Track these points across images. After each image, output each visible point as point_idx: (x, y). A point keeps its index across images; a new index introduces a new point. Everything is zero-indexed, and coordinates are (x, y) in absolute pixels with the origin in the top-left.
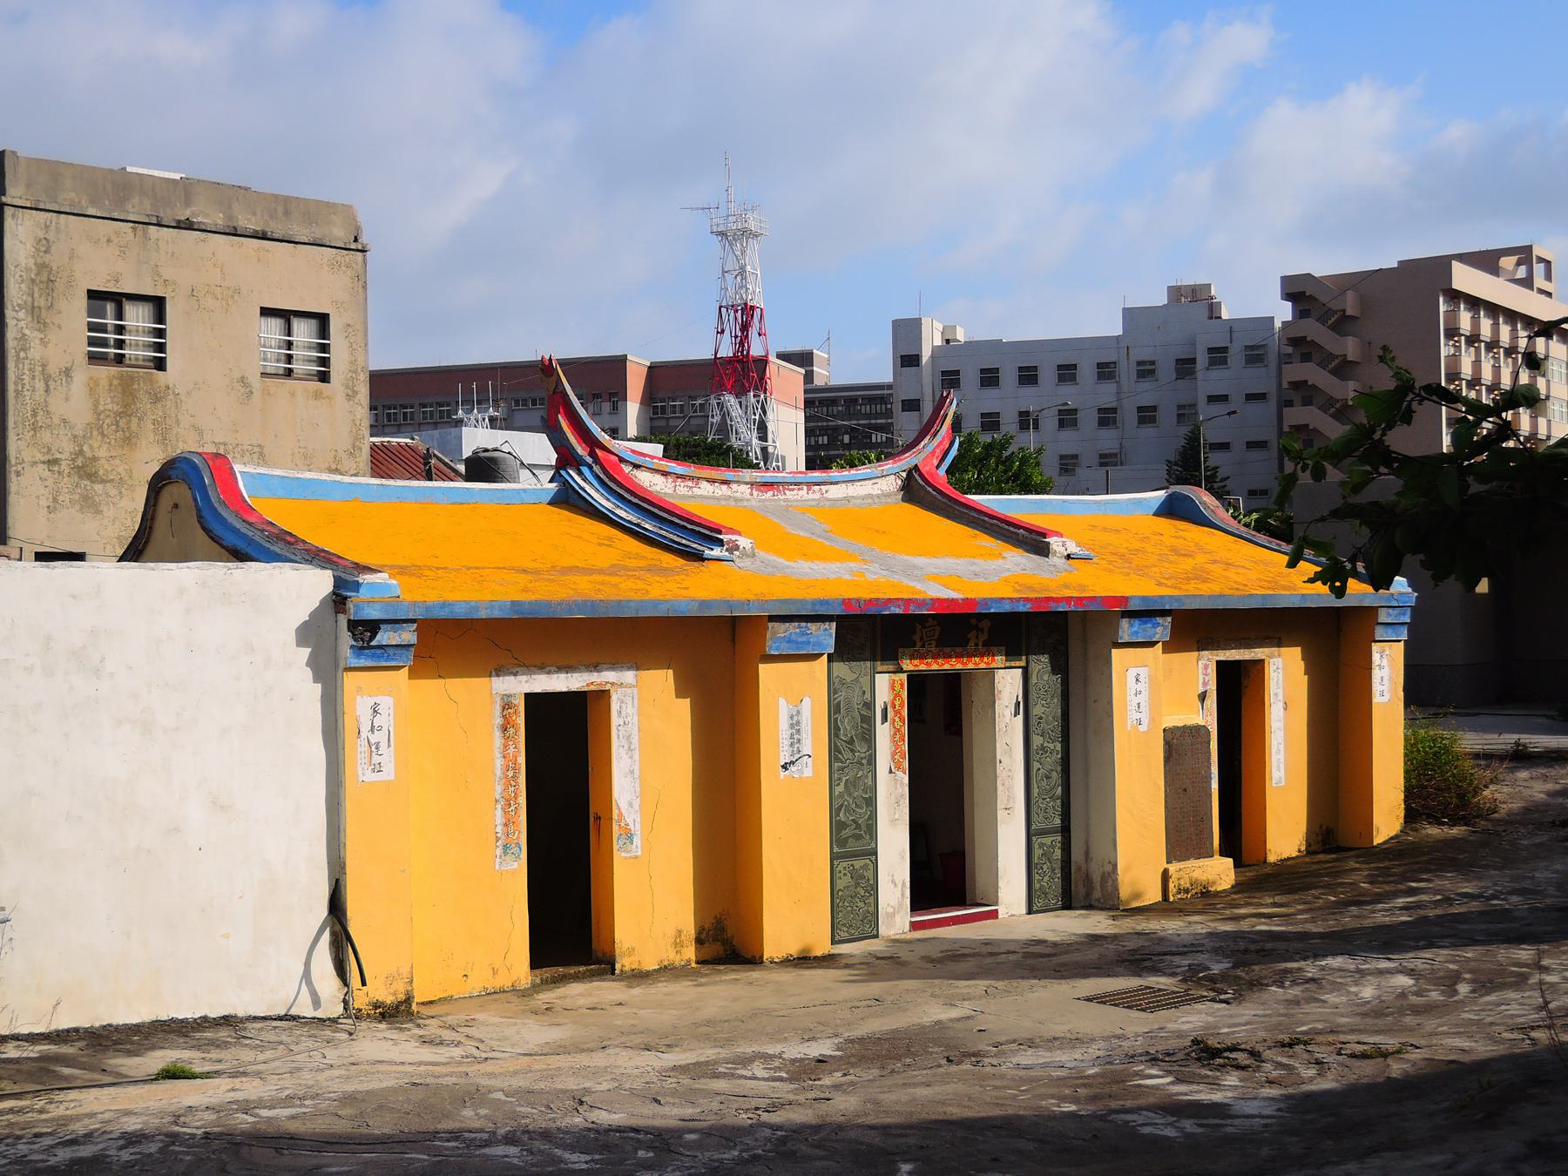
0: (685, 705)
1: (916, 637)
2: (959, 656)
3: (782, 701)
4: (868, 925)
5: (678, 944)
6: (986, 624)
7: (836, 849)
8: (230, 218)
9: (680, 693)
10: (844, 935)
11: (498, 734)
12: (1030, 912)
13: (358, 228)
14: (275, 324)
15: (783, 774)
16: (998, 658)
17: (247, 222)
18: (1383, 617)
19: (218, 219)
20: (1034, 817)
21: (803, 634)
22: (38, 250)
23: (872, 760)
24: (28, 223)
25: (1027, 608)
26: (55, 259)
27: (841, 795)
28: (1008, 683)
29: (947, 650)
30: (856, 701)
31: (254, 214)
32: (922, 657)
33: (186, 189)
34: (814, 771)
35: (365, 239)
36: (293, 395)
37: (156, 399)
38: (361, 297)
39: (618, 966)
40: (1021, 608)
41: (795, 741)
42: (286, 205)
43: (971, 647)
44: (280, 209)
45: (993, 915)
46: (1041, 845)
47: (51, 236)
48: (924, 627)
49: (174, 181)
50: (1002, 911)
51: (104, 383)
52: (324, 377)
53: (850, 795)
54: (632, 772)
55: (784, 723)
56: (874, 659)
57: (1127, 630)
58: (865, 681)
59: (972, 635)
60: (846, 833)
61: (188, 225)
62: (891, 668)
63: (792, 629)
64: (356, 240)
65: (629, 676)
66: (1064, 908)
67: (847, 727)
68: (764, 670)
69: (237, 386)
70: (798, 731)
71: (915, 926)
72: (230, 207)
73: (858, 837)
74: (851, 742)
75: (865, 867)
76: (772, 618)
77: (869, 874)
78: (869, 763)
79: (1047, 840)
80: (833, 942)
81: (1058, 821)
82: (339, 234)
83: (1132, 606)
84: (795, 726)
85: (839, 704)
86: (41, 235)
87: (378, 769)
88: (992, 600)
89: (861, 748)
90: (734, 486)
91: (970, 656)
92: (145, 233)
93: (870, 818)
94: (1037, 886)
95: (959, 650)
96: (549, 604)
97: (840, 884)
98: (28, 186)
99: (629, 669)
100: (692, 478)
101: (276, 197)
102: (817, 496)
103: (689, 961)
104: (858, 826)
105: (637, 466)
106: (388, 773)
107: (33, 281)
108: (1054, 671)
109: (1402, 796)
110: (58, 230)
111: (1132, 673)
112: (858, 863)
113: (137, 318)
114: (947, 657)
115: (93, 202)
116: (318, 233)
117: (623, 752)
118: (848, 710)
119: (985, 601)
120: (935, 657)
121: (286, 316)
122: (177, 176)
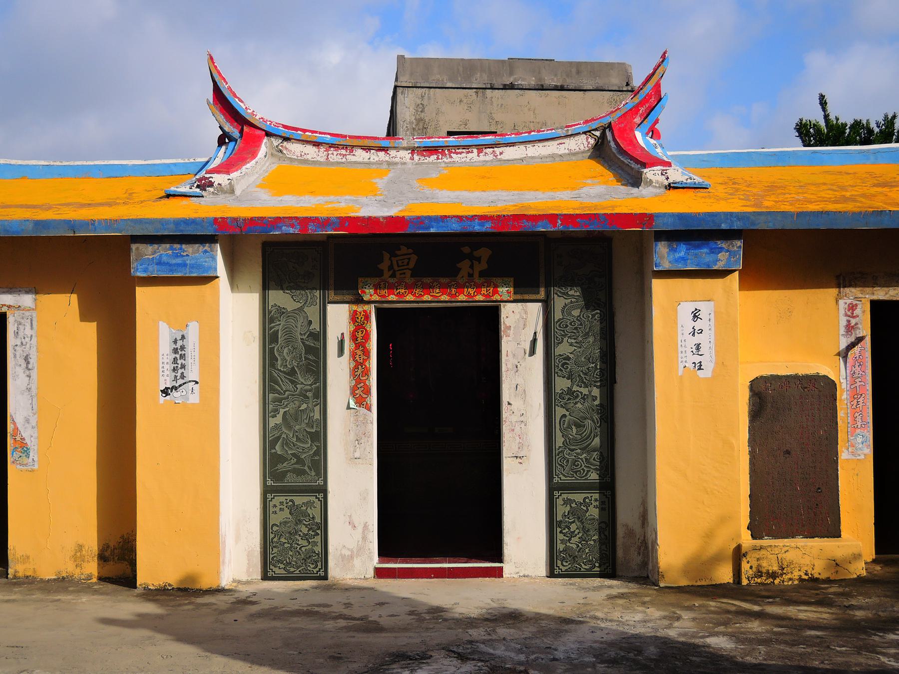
0: (91, 328)
1: (384, 266)
2: (444, 287)
3: (163, 327)
4: (315, 564)
5: (78, 556)
6: (484, 253)
7: (269, 482)
8: (540, 80)
9: (85, 316)
10: (279, 571)
12: (552, 574)
15: (162, 399)
16: (503, 290)
17: (551, 80)
19: (533, 82)
20: (557, 469)
21: (177, 256)
22: (417, 111)
24: (410, 96)
25: (487, 227)
26: (427, 116)
27: (277, 426)
28: (521, 322)
29: (428, 280)
30: (299, 331)
31: (556, 75)
32: (391, 288)
33: (511, 64)
34: (201, 397)
39: (11, 571)
40: (477, 228)
42: (578, 67)
44: (574, 70)
45: (498, 573)
47: (425, 102)
50: (508, 568)
53: (290, 428)
54: (29, 390)
55: (165, 348)
56: (324, 287)
57: (664, 255)
58: (312, 312)
59: (464, 265)
61: (511, 87)
62: (348, 298)
63: (163, 251)
64: (628, 84)
65: (27, 300)
66: (602, 575)
67: (286, 357)
68: (143, 294)
70: (183, 357)
71: (380, 573)
72: (539, 73)
74: (292, 372)
75: (309, 504)
77: (315, 512)
79: (578, 497)
80: (265, 577)
81: (594, 476)
82: (615, 81)
83: (659, 226)
84: (179, 352)
85: (276, 333)
86: (419, 102)
88: (430, 218)
89: (305, 381)
90: (393, 153)
91: (460, 287)
92: (484, 94)
93: (317, 453)
94: (561, 547)
95: (444, 280)
97: (274, 519)
98: (411, 74)
99: (27, 292)
101: (571, 63)
102: (491, 157)
103: (89, 577)
104: (300, 461)
105: (286, 139)
107: (414, 129)
108: (590, 303)
110: (429, 98)
111: (685, 310)
112: (299, 500)
114: (427, 288)
115: (450, 80)
116: (600, 82)
117: (20, 371)
118: (288, 341)
119: (420, 220)
120: (410, 288)
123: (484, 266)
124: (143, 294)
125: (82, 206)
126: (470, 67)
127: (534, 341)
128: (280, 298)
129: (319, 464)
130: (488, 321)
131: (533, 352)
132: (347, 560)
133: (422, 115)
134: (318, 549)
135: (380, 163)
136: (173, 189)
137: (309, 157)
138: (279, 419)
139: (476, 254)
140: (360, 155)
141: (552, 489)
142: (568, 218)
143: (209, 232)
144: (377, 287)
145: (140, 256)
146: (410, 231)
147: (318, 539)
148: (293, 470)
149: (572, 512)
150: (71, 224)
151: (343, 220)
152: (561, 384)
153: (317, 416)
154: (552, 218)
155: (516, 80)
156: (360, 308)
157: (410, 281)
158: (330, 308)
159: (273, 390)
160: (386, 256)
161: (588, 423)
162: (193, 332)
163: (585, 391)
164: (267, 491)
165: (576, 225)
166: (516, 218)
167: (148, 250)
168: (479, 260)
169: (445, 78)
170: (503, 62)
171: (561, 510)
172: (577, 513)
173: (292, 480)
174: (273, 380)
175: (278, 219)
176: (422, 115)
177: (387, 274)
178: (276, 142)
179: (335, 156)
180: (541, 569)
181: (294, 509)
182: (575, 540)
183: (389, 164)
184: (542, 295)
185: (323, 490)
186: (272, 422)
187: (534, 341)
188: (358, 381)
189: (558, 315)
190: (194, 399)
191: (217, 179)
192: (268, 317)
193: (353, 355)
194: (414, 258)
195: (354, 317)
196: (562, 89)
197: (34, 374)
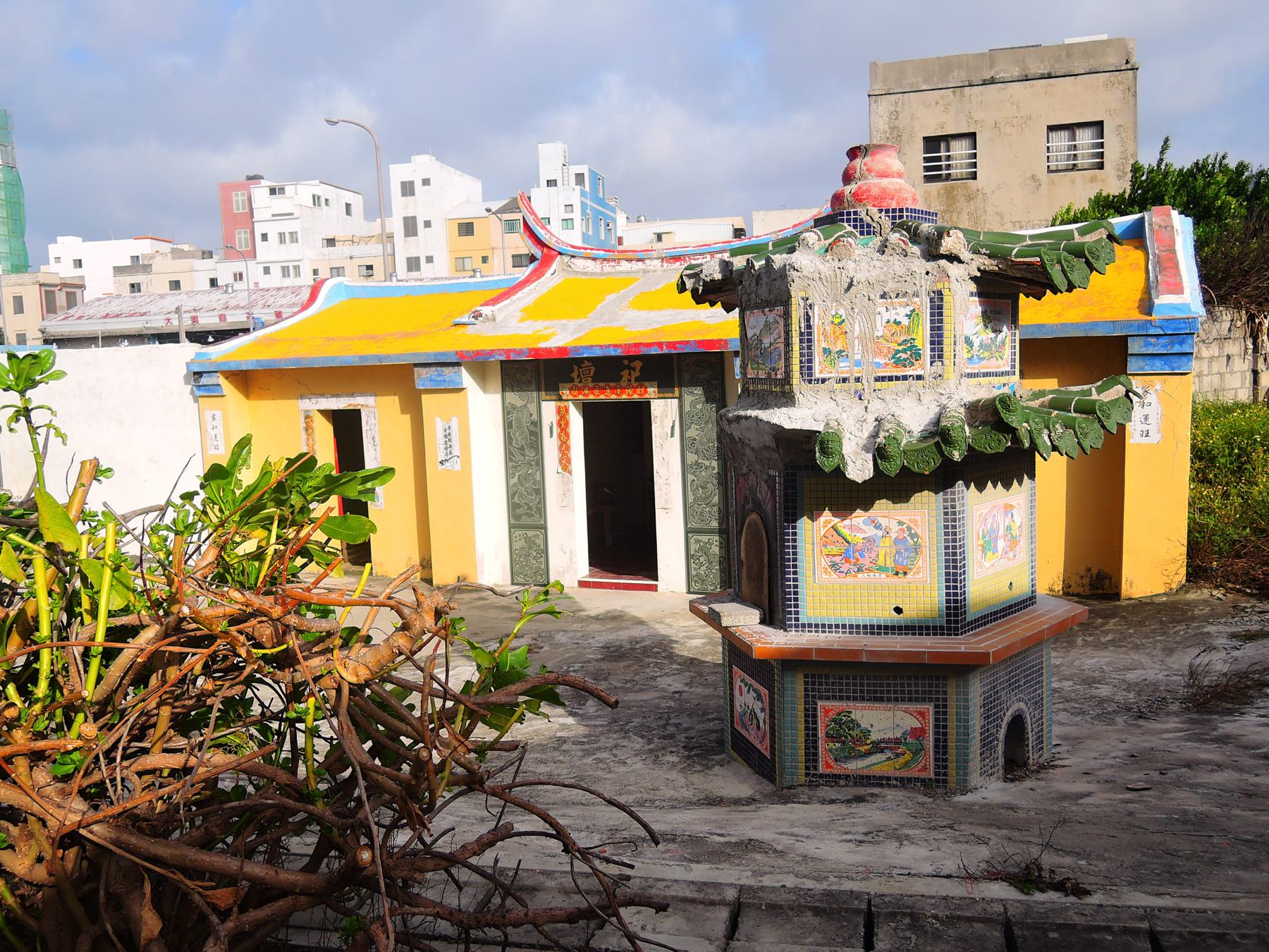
1: (575, 375)
3: (438, 420)
6: (638, 364)
11: (303, 432)
13: (1128, 54)
14: (1064, 135)
15: (440, 467)
16: (650, 390)
17: (1036, 68)
18: (1134, 347)
19: (1016, 72)
23: (540, 463)
25: (619, 352)
26: (901, 123)
28: (665, 413)
29: (602, 384)
30: (525, 421)
31: (1042, 62)
32: (580, 389)
35: (1134, 60)
36: (1073, 182)
37: (970, 198)
38: (1132, 103)
40: (613, 353)
41: (448, 447)
43: (624, 383)
44: (1064, 54)
46: (697, 541)
48: (580, 367)
49: (1103, 41)
50: (660, 584)
51: (935, 193)
52: (1101, 166)
55: (440, 434)
56: (539, 390)
58: (532, 407)
59: (625, 373)
60: (519, 511)
61: (992, 81)
62: (554, 397)
64: (1127, 62)
69: (1029, 182)
73: (530, 515)
74: (522, 449)
75: (536, 536)
76: (416, 365)
77: (540, 542)
78: (537, 464)
79: (705, 538)
80: (513, 584)
81: (715, 524)
82: (1113, 60)
84: (448, 436)
87: (217, 448)
89: (530, 454)
90: (648, 262)
91: (623, 388)
92: (962, 95)
94: (694, 573)
95: (612, 384)
96: (275, 361)
98: (885, 81)
100: (614, 260)
104: (529, 508)
106: (1155, 437)
108: (709, 399)
109: (1184, 550)
110: (903, 104)
112: (530, 533)
113: (959, 149)
114: (603, 389)
115: (925, 82)
116: (1094, 63)
117: (371, 446)
118: (519, 427)
119: (576, 349)
121: (1071, 128)
122: (1104, 37)
123: (637, 373)
124: (425, 398)
125: (406, 335)
126: (948, 64)
127: (673, 427)
128: (513, 397)
129: (541, 509)
130: (642, 410)
131: (672, 436)
132: (849, 559)
133: (897, 123)
134: (543, 566)
135: (637, 272)
136: (458, 320)
137: (589, 270)
138: (515, 480)
139: (632, 365)
140: (625, 266)
141: (688, 531)
142: (671, 345)
143: (454, 360)
144: (571, 389)
145: (419, 375)
146: (571, 356)
147: (542, 560)
148: (527, 513)
149: (701, 549)
150: (378, 357)
151: (531, 350)
152: (691, 458)
153: (538, 478)
154: (660, 345)
155: (997, 73)
156: (562, 404)
157: (591, 385)
158: (544, 404)
159: (511, 460)
160: (576, 367)
161: (710, 485)
162: (455, 423)
163: (707, 463)
164: (511, 527)
165: (676, 348)
166: (637, 345)
167: (423, 371)
168: (634, 369)
169: (920, 80)
170: (983, 55)
171: (694, 547)
172: (704, 550)
173: (525, 520)
174: (511, 453)
175: (493, 351)
176: (897, 123)
177: (577, 380)
178: (566, 259)
179: (607, 267)
180: (684, 590)
181: (527, 539)
182: (703, 568)
183: (645, 272)
184: (677, 394)
185: (544, 527)
186: (512, 481)
187: (673, 427)
188: (564, 454)
189: (687, 408)
190: (458, 467)
191: (486, 310)
192: (507, 411)
193: (559, 436)
194: (593, 369)
195: (559, 411)
196: (1050, 77)
197: (378, 448)
